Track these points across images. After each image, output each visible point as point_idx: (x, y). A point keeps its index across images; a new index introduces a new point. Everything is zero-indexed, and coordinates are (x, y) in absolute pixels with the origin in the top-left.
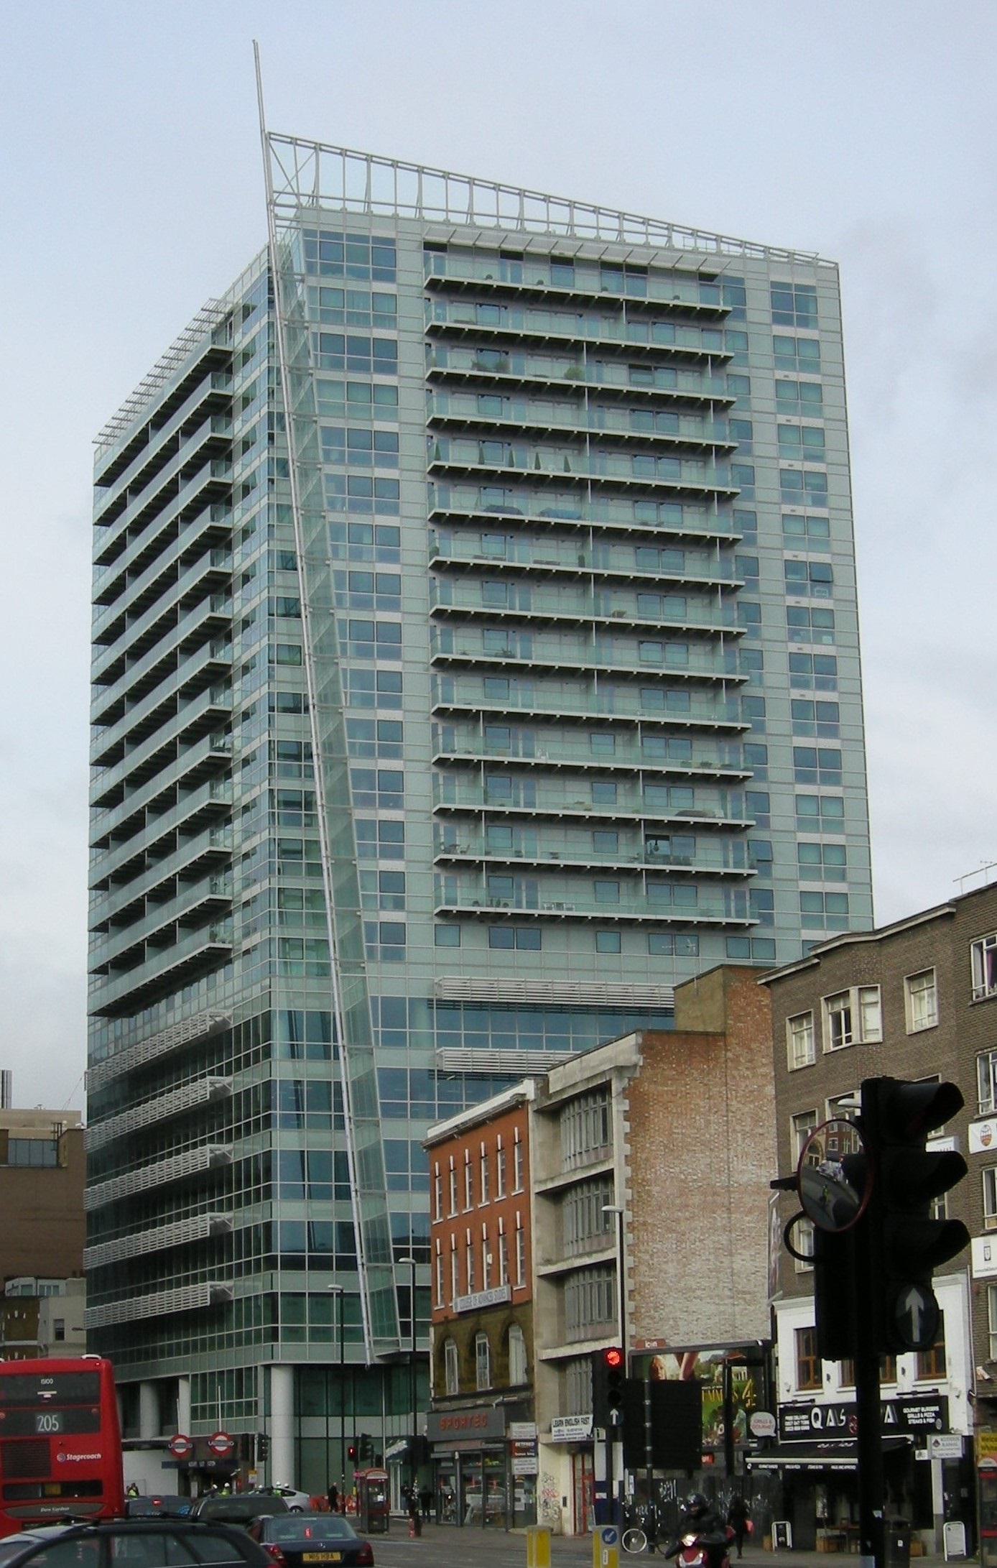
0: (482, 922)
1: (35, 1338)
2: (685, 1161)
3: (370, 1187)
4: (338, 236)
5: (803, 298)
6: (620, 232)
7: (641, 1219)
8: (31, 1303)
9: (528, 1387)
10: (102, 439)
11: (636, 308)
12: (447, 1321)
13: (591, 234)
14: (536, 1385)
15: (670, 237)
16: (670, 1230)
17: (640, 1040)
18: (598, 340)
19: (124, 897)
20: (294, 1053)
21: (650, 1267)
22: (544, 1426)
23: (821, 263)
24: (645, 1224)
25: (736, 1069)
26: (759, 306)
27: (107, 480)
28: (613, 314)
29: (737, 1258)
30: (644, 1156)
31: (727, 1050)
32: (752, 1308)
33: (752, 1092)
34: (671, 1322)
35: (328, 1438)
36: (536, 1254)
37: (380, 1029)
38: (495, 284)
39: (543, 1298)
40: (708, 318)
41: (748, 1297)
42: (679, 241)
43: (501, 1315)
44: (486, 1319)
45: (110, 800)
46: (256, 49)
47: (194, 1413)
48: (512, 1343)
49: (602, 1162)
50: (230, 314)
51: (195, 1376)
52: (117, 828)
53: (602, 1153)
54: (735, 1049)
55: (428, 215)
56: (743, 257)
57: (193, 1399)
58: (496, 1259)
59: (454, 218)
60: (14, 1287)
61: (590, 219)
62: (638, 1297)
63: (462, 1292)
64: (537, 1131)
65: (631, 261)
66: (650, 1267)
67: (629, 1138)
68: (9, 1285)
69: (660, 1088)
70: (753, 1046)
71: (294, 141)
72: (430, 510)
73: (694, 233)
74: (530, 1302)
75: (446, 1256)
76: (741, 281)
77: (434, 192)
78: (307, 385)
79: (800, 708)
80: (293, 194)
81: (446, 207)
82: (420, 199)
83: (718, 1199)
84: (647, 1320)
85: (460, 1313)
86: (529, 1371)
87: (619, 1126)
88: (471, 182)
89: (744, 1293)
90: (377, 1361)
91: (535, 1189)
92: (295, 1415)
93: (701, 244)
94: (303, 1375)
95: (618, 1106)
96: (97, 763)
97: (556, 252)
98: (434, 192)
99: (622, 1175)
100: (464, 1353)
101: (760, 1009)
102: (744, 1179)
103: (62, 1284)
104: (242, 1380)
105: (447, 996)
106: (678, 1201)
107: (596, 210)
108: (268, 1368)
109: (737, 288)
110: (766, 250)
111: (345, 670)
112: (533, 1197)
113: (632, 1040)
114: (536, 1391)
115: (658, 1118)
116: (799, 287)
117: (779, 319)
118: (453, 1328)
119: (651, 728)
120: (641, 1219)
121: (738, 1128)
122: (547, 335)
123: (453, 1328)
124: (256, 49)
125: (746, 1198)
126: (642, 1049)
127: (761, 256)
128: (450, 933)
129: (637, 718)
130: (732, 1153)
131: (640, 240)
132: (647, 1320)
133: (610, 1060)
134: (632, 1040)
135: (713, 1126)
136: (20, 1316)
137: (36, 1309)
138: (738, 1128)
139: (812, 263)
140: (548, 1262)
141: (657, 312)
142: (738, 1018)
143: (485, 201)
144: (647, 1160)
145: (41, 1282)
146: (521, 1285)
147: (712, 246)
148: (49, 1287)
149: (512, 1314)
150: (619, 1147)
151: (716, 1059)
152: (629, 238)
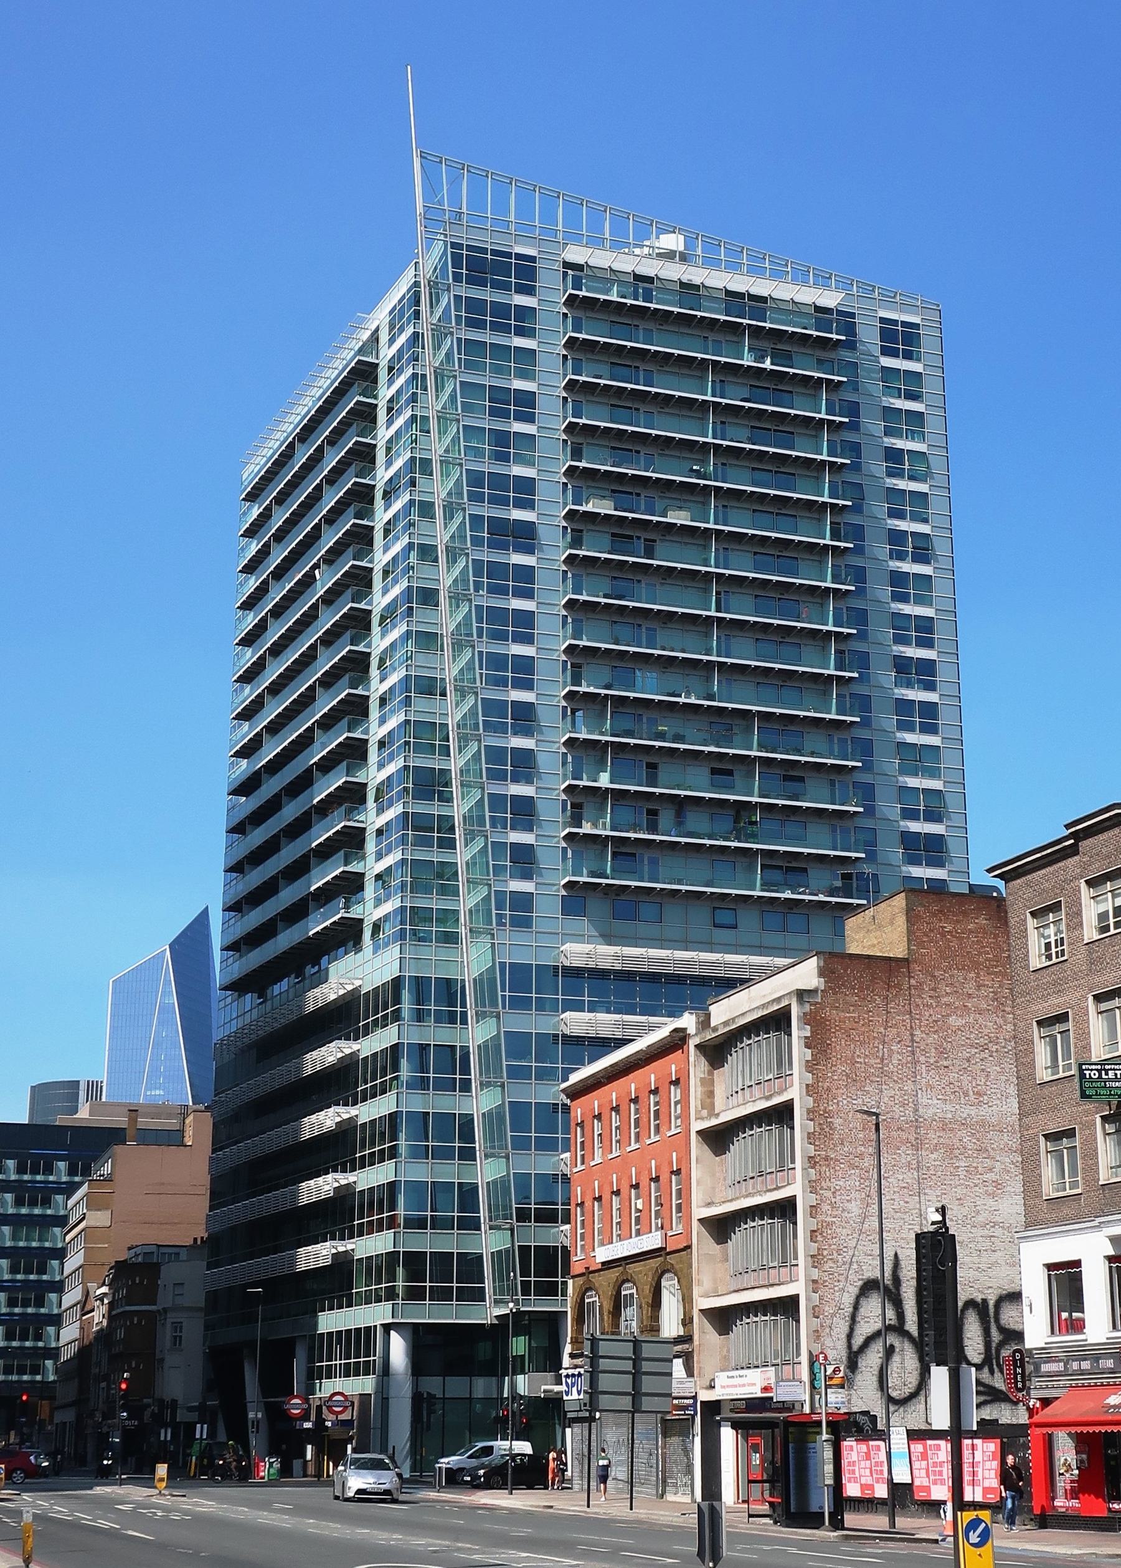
1: (155, 1304)
2: (868, 1092)
3: (493, 1147)
9: (687, 1339)
12: (588, 1272)
14: (696, 1337)
16: (853, 1166)
17: (822, 964)
19: (257, 877)
21: (833, 1206)
31: (910, 977)
33: (936, 1021)
36: (696, 1196)
37: (507, 994)
44: (633, 1268)
45: (246, 787)
48: (665, 1295)
49: (780, 1093)
52: (253, 813)
54: (918, 976)
62: (819, 1238)
64: (697, 1067)
66: (833, 1206)
67: (810, 1066)
69: (842, 1015)
78: (448, 389)
83: (904, 1136)
84: (830, 1263)
85: (603, 1264)
86: (687, 1321)
90: (495, 1322)
91: (697, 1126)
92: (413, 1374)
95: (798, 1032)
96: (231, 831)
101: (943, 935)
111: (481, 653)
112: (693, 1136)
113: (812, 964)
115: (839, 1045)
116: (905, 324)
118: (596, 1279)
121: (922, 1059)
123: (596, 1279)
126: (822, 973)
132: (830, 1263)
134: (812, 964)
135: (896, 1056)
136: (141, 1282)
138: (922, 1059)
142: (921, 945)
144: (829, 1089)
146: (677, 1228)
151: (898, 986)
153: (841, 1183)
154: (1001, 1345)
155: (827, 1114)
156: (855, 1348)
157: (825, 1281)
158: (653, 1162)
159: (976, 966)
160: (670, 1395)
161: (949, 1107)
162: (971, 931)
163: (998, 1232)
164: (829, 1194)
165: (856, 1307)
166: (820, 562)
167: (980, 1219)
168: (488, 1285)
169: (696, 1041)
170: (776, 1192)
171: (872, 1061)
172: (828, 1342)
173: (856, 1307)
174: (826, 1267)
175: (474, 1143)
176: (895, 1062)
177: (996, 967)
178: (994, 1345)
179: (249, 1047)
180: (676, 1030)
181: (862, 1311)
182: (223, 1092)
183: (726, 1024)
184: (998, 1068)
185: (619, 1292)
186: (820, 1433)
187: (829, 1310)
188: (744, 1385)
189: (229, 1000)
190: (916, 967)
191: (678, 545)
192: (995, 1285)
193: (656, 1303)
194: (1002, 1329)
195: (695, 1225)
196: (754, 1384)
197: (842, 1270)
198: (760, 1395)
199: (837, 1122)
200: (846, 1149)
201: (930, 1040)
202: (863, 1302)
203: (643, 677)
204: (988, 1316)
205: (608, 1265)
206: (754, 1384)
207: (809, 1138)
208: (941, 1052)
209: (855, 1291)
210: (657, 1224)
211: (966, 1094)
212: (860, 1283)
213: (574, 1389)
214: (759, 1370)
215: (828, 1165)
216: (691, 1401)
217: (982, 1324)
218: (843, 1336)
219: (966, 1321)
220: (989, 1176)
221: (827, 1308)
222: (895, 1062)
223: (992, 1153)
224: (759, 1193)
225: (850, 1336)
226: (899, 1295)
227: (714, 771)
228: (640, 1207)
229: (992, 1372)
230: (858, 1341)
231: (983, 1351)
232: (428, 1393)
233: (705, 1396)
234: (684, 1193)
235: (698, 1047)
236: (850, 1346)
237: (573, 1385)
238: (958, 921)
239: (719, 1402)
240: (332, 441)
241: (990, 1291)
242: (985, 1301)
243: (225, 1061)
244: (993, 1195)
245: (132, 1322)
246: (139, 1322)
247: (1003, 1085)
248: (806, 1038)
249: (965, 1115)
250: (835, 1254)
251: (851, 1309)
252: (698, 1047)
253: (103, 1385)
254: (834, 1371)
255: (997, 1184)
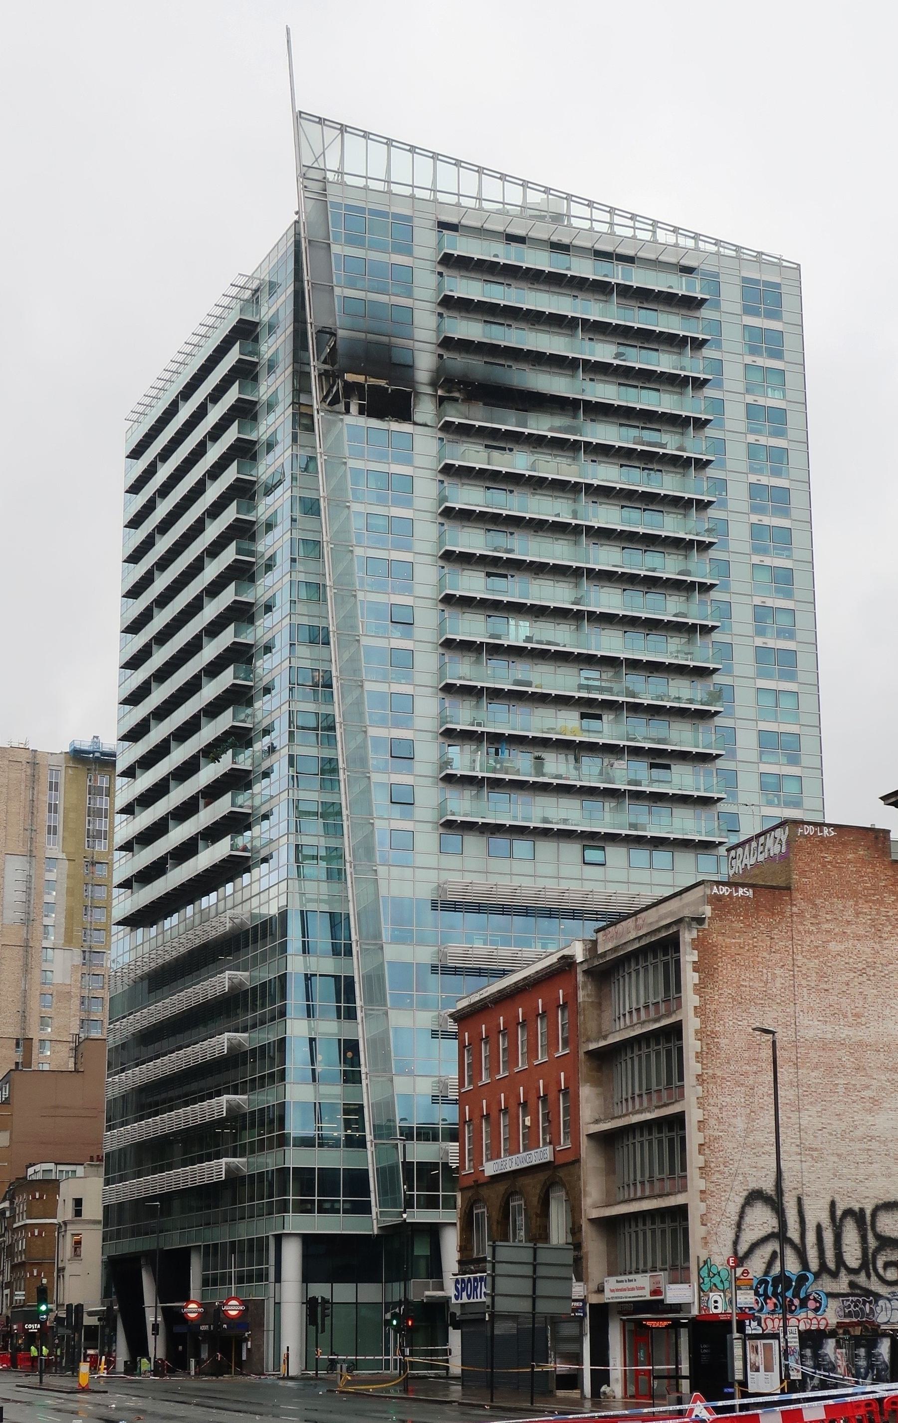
0: (482, 833)
4: (362, 210)
5: (771, 293)
6: (611, 224)
7: (710, 1072)
8: (51, 1186)
10: (135, 417)
11: (627, 292)
12: (477, 1185)
13: (586, 225)
15: (654, 232)
18: (592, 318)
20: (306, 949)
21: (720, 1121)
22: (593, 1286)
23: (785, 264)
24: (714, 1076)
25: (802, 923)
26: (731, 297)
27: (136, 453)
28: (603, 298)
29: (804, 1114)
30: (713, 1007)
31: (792, 905)
32: (819, 1165)
33: (817, 947)
34: (741, 1178)
35: (332, 1303)
38: (502, 261)
39: (591, 1161)
40: (690, 304)
41: (815, 1154)
42: (663, 237)
43: (542, 1177)
46: (288, 34)
47: (205, 1282)
50: (256, 291)
51: (207, 1247)
52: (143, 757)
53: (663, 1008)
55: (442, 197)
56: (717, 253)
57: (205, 1268)
58: (535, 1121)
59: (465, 202)
60: (35, 1172)
61: (585, 212)
62: (707, 1151)
63: (495, 1155)
65: (620, 251)
66: (720, 1121)
67: (699, 989)
68: (31, 1171)
69: (728, 940)
70: (818, 901)
71: (321, 121)
72: (440, 462)
73: (676, 230)
74: (578, 1161)
75: (476, 1121)
76: (717, 275)
77: (447, 177)
79: (762, 653)
80: (324, 150)
81: (457, 191)
82: (434, 181)
84: (717, 1175)
85: (492, 1177)
86: (575, 1230)
87: (690, 978)
88: (480, 170)
89: (811, 1149)
92: (303, 1282)
93: (682, 241)
94: (309, 1242)
95: (689, 957)
97: (554, 239)
98: (447, 177)
99: (691, 1026)
100: (495, 1215)
102: (810, 1034)
103: (80, 1170)
104: (256, 1249)
105: (450, 898)
106: (746, 1055)
107: (590, 204)
108: (279, 1238)
109: (713, 281)
110: (738, 248)
114: (584, 1250)
115: (726, 970)
116: (766, 283)
117: (748, 310)
118: (484, 1192)
119: (634, 665)
120: (710, 1072)
121: (804, 983)
122: (548, 311)
123: (484, 1192)
124: (288, 34)
125: (812, 1054)
127: (733, 254)
128: (454, 839)
129: (622, 656)
130: (798, 1009)
131: (629, 232)
133: (671, 913)
135: (779, 981)
136: (41, 1197)
137: (57, 1190)
138: (804, 983)
139: (778, 264)
140: (597, 1122)
141: (643, 296)
143: (492, 189)
144: (716, 1011)
145: (60, 1167)
146: (564, 1144)
147: (690, 243)
148: (67, 1172)
149: (557, 1176)
150: (690, 999)
151: (782, 913)
152: (618, 230)
153: (728, 1100)
154: (877, 1250)
155: (714, 1035)
156: (741, 1253)
157: (713, 1192)
158: (541, 1081)
159: (855, 894)
160: (570, 1298)
161: (829, 1028)
162: (850, 862)
163: (874, 1145)
164: (715, 1110)
165: (742, 1215)
166: (685, 516)
167: (858, 1133)
168: (373, 1198)
169: (585, 967)
170: (665, 1108)
171: (756, 985)
172: (715, 1248)
173: (742, 1215)
174: (714, 1178)
175: (359, 1066)
176: (778, 985)
177: (874, 895)
178: (871, 1251)
179: (142, 978)
180: (563, 957)
181: (748, 1219)
182: (117, 1020)
183: (614, 949)
184: (875, 991)
185: (507, 1204)
186: (731, 1332)
187: (715, 1218)
188: (633, 1289)
189: (121, 935)
190: (797, 895)
191: (550, 499)
192: (871, 1195)
193: (545, 1213)
194: (878, 1237)
195: (584, 1142)
196: (644, 1288)
197: (728, 1181)
198: (648, 1297)
199: (723, 1042)
200: (732, 1067)
201: (812, 965)
202: (748, 1210)
203: (517, 626)
204: (865, 1223)
205: (495, 1178)
206: (644, 1288)
207: (697, 1057)
208: (822, 976)
209: (740, 1201)
210: (544, 1139)
211: (845, 1017)
212: (745, 1194)
213: (464, 1294)
214: (648, 1275)
215: (715, 1083)
216: (581, 1304)
217: (860, 1231)
218: (730, 1244)
219: (844, 1228)
220: (867, 1093)
221: (714, 1217)
222: (778, 985)
223: (869, 1071)
224: (648, 1110)
225: (736, 1243)
226: (782, 1204)
227: (583, 716)
228: (528, 1123)
229: (868, 1276)
230: (743, 1248)
231: (860, 1257)
232: (322, 1297)
233: (594, 1299)
234: (573, 1110)
235: (585, 972)
236: (735, 1252)
237: (463, 1290)
238: (837, 852)
239: (607, 1304)
240: (216, 396)
241: (867, 1200)
242: (862, 1210)
243: (120, 991)
244: (870, 1111)
245: (33, 1234)
246: (40, 1234)
247: (880, 1007)
248: (694, 962)
249: (843, 1036)
250: (722, 1167)
251: (737, 1218)
252: (585, 972)
253: (7, 1291)
254: (743, 1273)
255: (874, 1101)
